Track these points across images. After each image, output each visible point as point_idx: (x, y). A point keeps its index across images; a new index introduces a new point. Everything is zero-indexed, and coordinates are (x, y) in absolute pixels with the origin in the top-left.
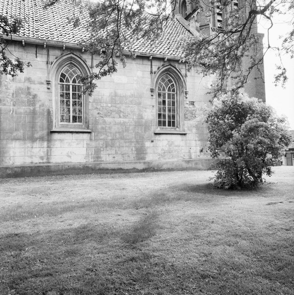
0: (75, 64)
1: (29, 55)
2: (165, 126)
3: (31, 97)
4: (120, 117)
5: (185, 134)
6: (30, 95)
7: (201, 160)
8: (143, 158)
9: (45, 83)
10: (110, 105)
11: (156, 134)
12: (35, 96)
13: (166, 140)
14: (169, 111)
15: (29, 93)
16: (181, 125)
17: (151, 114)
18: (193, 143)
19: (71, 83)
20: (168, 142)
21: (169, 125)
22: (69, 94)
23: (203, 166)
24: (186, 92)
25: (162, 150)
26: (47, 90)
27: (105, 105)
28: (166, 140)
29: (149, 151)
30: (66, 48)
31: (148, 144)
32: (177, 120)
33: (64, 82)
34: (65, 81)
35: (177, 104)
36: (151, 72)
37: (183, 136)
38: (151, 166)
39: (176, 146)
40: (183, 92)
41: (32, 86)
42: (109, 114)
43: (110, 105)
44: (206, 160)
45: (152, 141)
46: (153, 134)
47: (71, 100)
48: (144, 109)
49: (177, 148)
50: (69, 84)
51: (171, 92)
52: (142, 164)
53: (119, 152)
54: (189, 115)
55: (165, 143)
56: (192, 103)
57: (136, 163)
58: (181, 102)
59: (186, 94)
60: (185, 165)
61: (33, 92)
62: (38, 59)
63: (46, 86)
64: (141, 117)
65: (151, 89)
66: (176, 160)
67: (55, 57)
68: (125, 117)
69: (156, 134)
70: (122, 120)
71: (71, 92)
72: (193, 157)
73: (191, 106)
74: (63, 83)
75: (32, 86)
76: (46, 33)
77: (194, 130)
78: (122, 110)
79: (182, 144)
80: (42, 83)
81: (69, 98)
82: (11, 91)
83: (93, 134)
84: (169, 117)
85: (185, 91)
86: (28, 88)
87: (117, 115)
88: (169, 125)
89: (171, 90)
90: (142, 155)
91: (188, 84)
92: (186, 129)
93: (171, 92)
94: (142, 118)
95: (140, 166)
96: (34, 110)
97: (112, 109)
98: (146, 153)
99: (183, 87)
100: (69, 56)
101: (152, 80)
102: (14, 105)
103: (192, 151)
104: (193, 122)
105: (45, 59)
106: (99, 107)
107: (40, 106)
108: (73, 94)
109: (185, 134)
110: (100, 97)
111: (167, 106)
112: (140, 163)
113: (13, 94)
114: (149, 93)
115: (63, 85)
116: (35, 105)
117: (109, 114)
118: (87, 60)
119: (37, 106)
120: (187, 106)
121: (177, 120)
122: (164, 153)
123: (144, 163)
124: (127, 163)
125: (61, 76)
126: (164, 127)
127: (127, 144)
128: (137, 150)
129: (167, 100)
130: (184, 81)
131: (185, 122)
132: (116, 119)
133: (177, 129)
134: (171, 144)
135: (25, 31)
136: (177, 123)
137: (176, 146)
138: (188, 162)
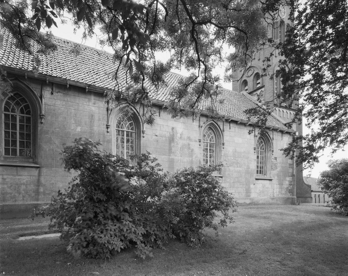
0: (212, 128)
1: (189, 120)
2: (9, 155)
3: (190, 151)
4: (238, 167)
5: (271, 180)
6: (190, 149)
7: (279, 198)
8: (249, 196)
9: (198, 141)
10: (232, 158)
11: (256, 179)
12: (192, 150)
13: (262, 183)
14: (261, 163)
15: (189, 148)
16: (268, 173)
17: (253, 166)
18: (275, 186)
19: (209, 141)
20: (263, 185)
21: (260, 173)
22: (207, 149)
23: (280, 202)
24: (273, 150)
25: (259, 190)
26: (199, 146)
27: (230, 158)
28: (262, 183)
29: (252, 191)
30: (49, 82)
31: (252, 186)
32: (265, 170)
33: (9, 111)
34: (10, 110)
35: (265, 159)
36: (199, 126)
37: (271, 181)
38: (253, 201)
39: (266, 188)
40: (270, 150)
41: (191, 143)
42: (232, 165)
43: (232, 158)
44: (282, 198)
45: (254, 184)
46: (255, 179)
47: (209, 154)
48: (250, 162)
49: (267, 189)
50: (123, 130)
51: (262, 150)
52: (249, 200)
53: (237, 191)
54: (274, 167)
55: (261, 185)
56: (276, 158)
57: (246, 199)
58: (269, 157)
59: (273, 152)
60: (271, 201)
61: (192, 147)
62: (194, 123)
63: (198, 143)
64: (248, 167)
65: (254, 148)
66: (266, 197)
67: (203, 122)
68: (240, 167)
69: (256, 179)
70: (239, 169)
71: (209, 148)
72: (275, 195)
73: (275, 161)
74: (119, 129)
75: (191, 143)
76: (63, 72)
77: (276, 178)
78: (239, 162)
79: (270, 186)
80: (196, 141)
81: (207, 152)
82: (179, 146)
83: (223, 178)
84: (260, 167)
85: (272, 150)
86: (189, 145)
87: (236, 166)
88: (260, 173)
89: (25, 112)
90: (249, 194)
91: (274, 145)
92: (272, 176)
93: (262, 150)
94: (249, 168)
95: (248, 201)
96: (192, 159)
97: (233, 161)
98: (251, 193)
99: (270, 147)
100: (211, 122)
101: (255, 141)
102: (181, 156)
103: (275, 192)
104: (275, 172)
105: (198, 124)
106: (227, 159)
107: (195, 157)
108: (210, 149)
109: (271, 180)
110: (227, 152)
111: (259, 160)
112: (248, 199)
113: (181, 148)
114: (253, 151)
115: (119, 131)
116: (192, 157)
117: (232, 165)
118: (221, 125)
119: (194, 157)
120: (273, 160)
121: (265, 170)
122: (260, 192)
123: (250, 199)
124: (241, 199)
125: (24, 106)
126: (8, 156)
127: (241, 186)
128: (246, 190)
129: (259, 155)
130: (272, 143)
131: (272, 171)
132: (235, 168)
133: (265, 176)
134: (264, 186)
135: (48, 68)
136: (265, 172)
137: (266, 188)
138: (273, 199)
